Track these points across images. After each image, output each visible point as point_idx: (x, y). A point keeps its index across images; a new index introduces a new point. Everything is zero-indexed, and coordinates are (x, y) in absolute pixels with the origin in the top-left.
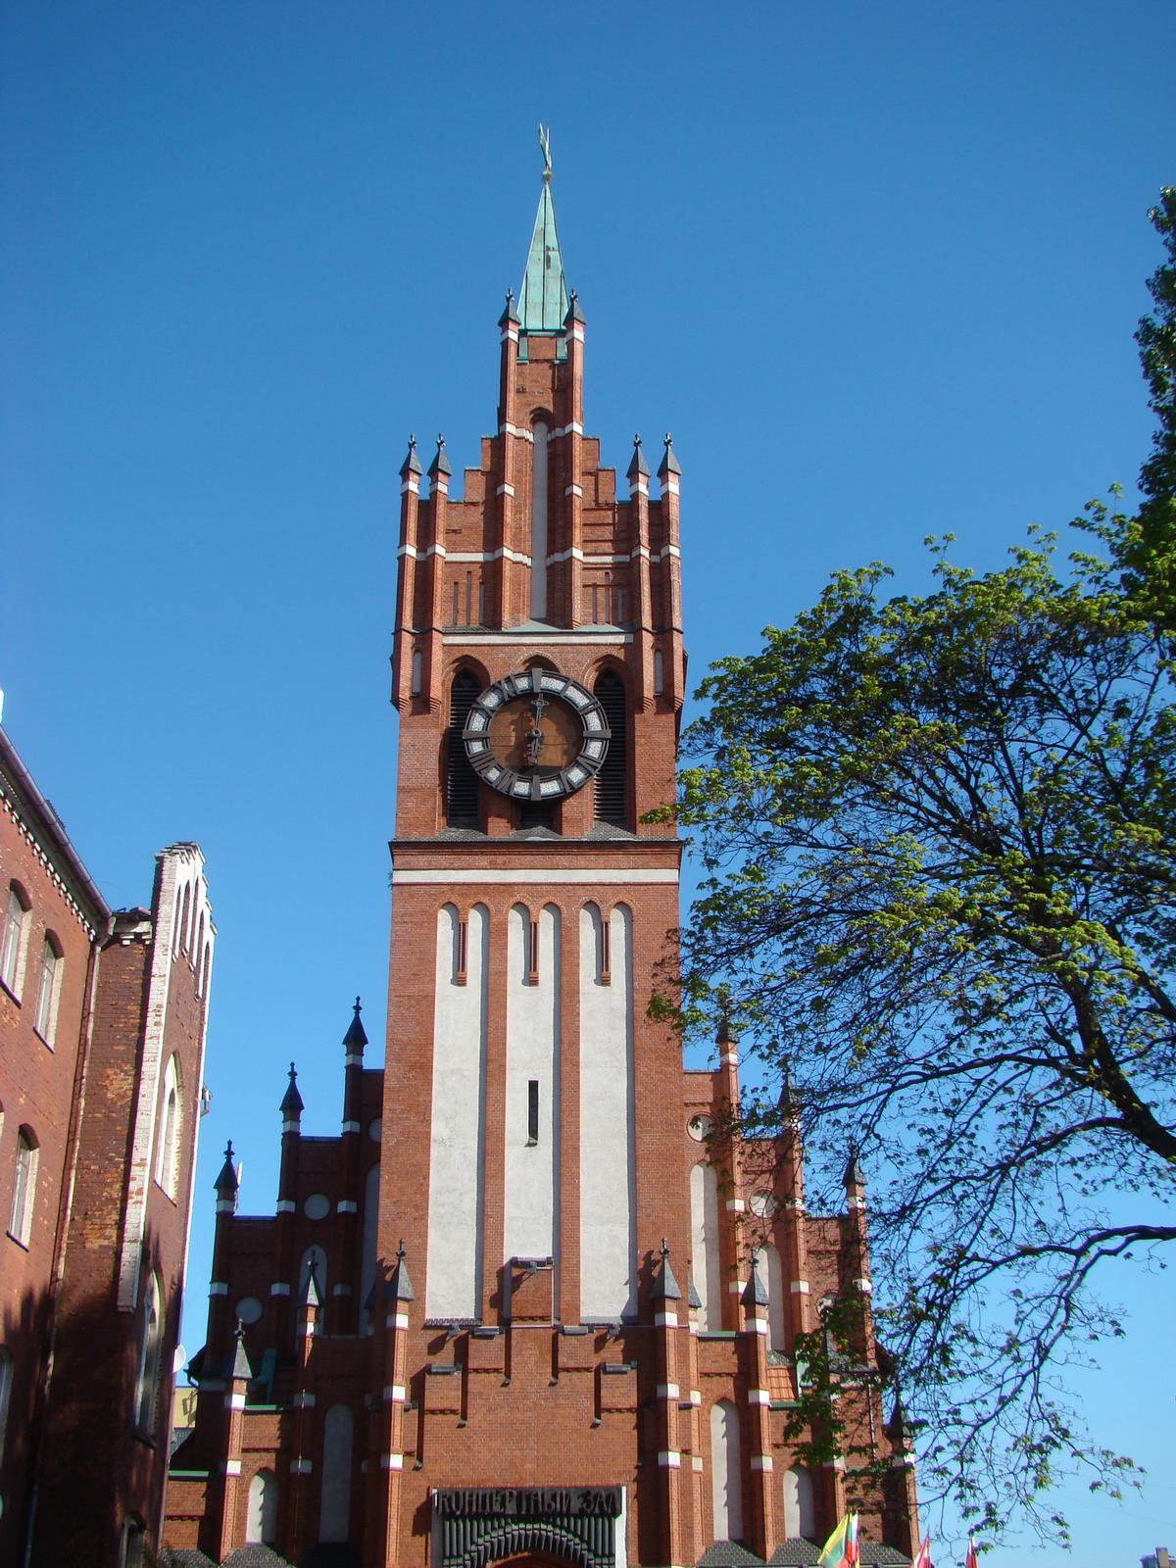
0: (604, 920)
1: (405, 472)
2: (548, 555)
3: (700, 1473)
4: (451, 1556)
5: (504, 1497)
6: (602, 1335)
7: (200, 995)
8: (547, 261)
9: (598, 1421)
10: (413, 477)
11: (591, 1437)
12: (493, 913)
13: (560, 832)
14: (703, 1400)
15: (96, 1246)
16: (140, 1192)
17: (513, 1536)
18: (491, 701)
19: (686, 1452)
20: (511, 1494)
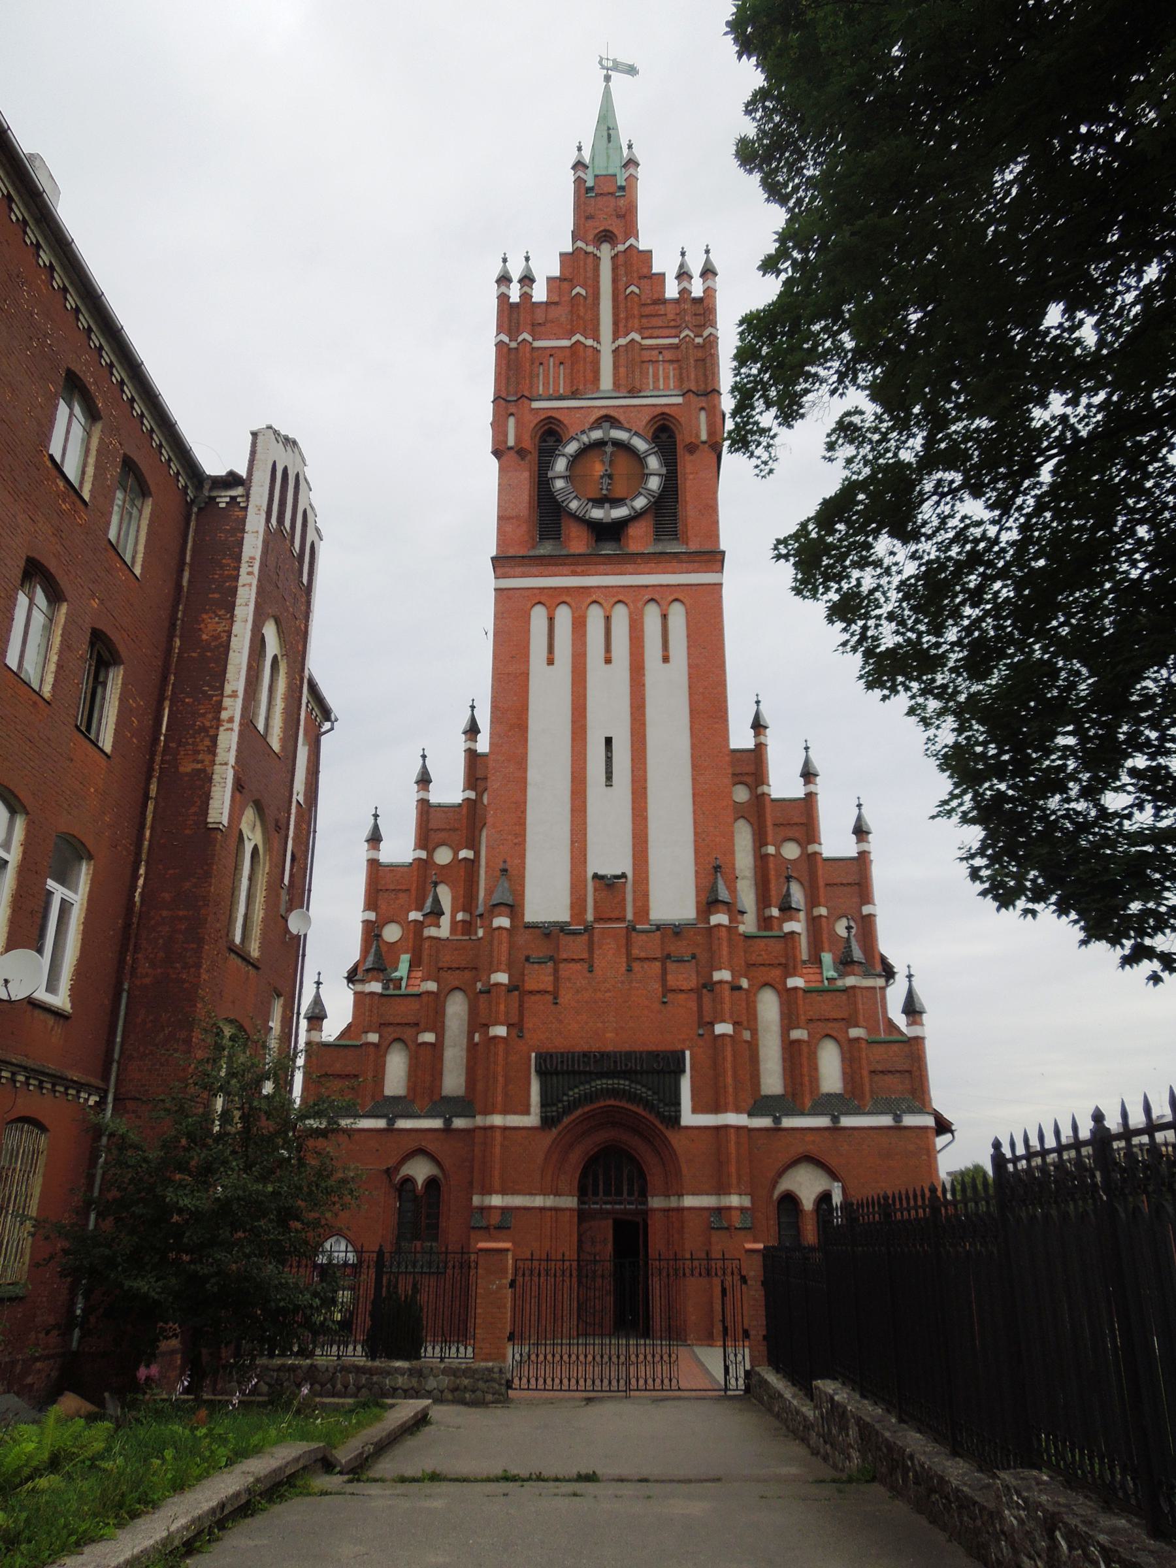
2: (613, 342)
14: (749, 985)
15: (189, 770)
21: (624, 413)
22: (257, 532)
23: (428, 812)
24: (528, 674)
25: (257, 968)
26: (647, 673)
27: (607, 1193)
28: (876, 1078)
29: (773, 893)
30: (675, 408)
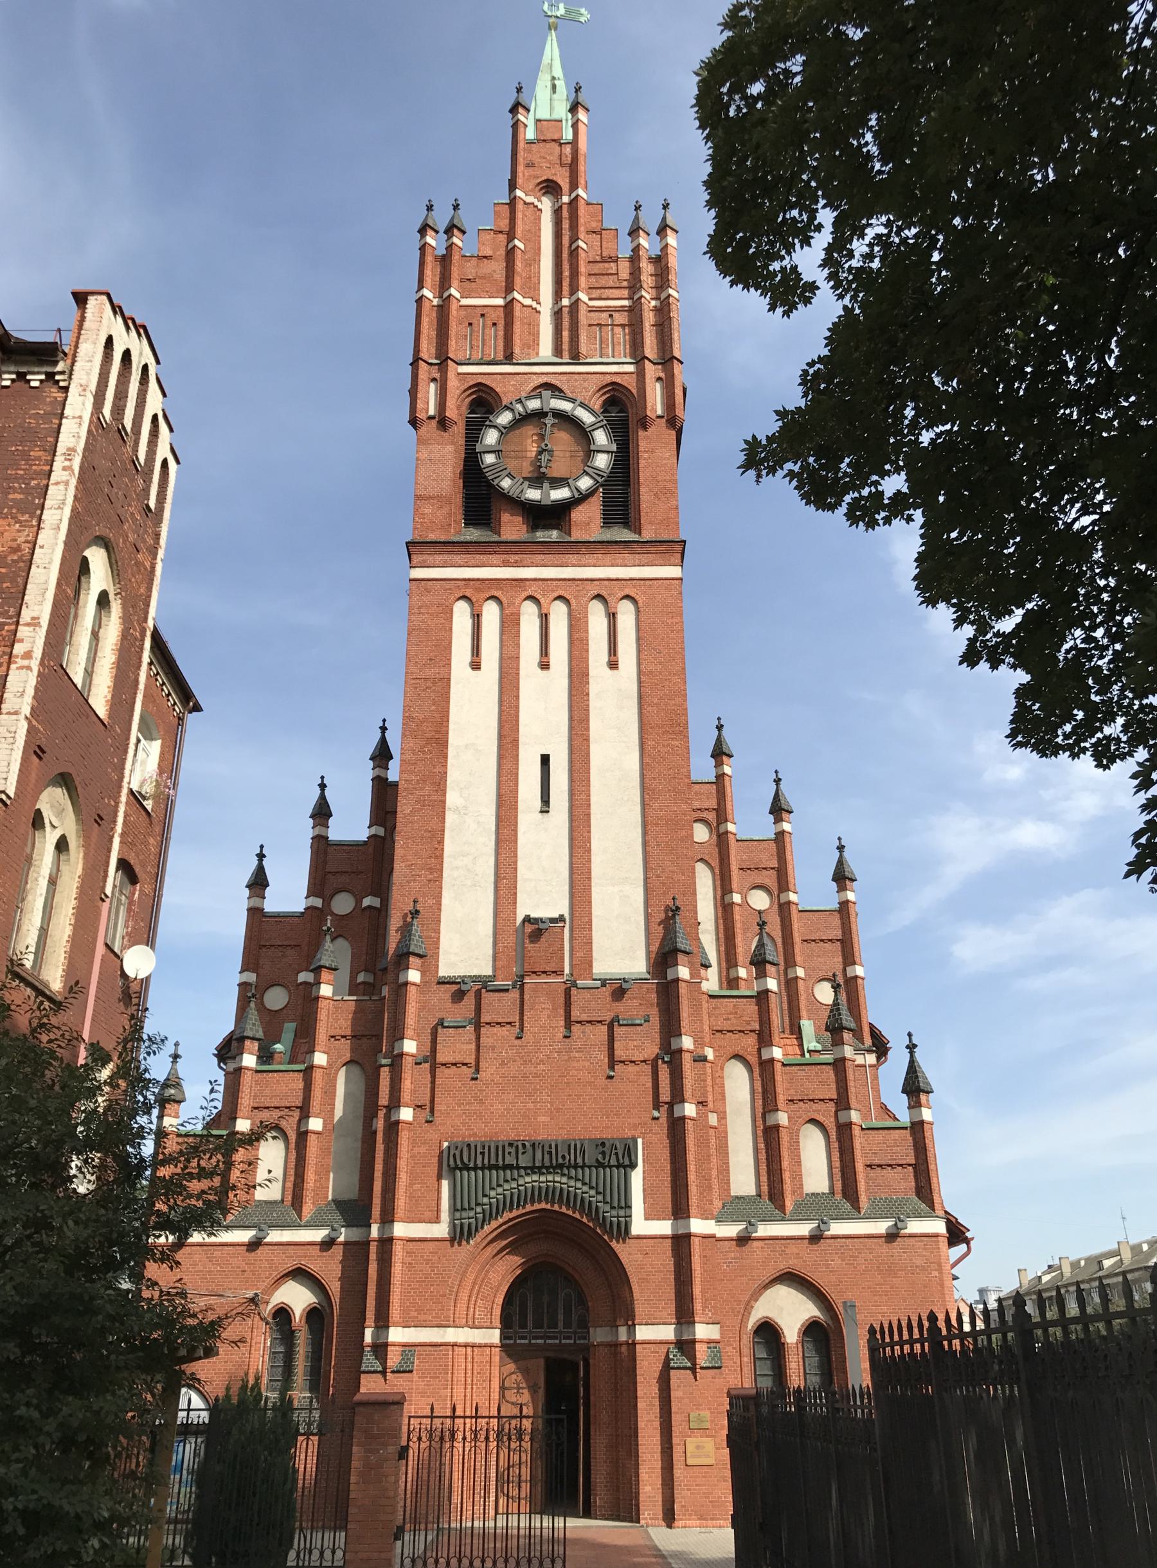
4: (463, 1209)
6: (619, 989)
7: (152, 504)
8: (554, 87)
10: (430, 232)
11: (605, 1089)
13: (570, 535)
16: (28, 655)
17: (526, 1188)
18: (505, 418)
19: (701, 1103)
21: (568, 381)
22: (80, 417)
23: (326, 852)
24: (449, 679)
26: (591, 681)
28: (872, 1173)
29: (740, 950)
30: (626, 377)
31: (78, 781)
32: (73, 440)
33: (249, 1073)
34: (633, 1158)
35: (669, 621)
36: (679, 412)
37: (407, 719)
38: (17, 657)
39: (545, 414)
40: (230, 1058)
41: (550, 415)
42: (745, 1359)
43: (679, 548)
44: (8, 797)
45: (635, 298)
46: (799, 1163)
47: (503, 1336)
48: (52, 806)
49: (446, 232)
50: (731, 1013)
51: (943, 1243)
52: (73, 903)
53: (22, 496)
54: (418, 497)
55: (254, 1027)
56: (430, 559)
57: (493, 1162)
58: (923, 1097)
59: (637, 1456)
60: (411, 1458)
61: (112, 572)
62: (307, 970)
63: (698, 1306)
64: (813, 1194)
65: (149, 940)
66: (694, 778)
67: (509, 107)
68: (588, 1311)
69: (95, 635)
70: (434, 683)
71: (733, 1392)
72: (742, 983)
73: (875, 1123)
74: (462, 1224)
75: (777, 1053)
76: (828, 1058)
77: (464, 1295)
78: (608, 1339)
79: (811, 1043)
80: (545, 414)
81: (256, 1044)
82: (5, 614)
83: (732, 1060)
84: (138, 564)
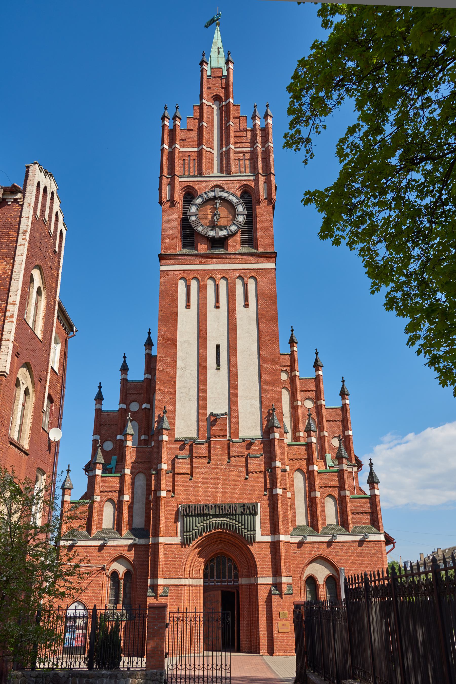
0: (246, 283)
1: (163, 118)
3: (290, 498)
4: (187, 532)
5: (209, 507)
6: (249, 443)
7: (57, 249)
8: (218, 52)
9: (247, 477)
10: (166, 119)
11: (245, 483)
12: (201, 281)
13: (227, 250)
16: (12, 316)
17: (213, 523)
18: (199, 201)
19: (284, 489)
20: (212, 506)
21: (226, 184)
22: (28, 217)
23: (127, 385)
24: (177, 313)
25: (27, 454)
27: (218, 577)
28: (354, 516)
29: (301, 425)
31: (32, 365)
32: (25, 227)
33: (99, 477)
34: (256, 510)
35: (270, 287)
36: (274, 197)
37: (160, 330)
38: (8, 317)
39: (216, 199)
40: (90, 470)
41: (219, 199)
42: (302, 591)
43: (274, 256)
44: (7, 374)
45: (255, 147)
46: (324, 512)
47: (204, 582)
48: (23, 376)
49: (173, 119)
50: (297, 452)
51: (383, 544)
52: (32, 414)
53: (6, 251)
54: (163, 235)
55: (100, 458)
56: (168, 262)
57: (199, 512)
58: (376, 485)
59: (259, 629)
60: (170, 628)
61: (42, 279)
62: (121, 434)
63: (283, 569)
64: (330, 525)
65: (59, 426)
66: (281, 353)
67: (199, 62)
68: (238, 571)
69: (36, 305)
70: (171, 315)
71: (296, 603)
72: (302, 439)
73: (356, 496)
74: (187, 538)
75: (316, 468)
76: (336, 469)
77: (188, 566)
78: (247, 582)
79: (330, 463)
80: (216, 199)
81: (101, 465)
82: (1, 299)
83: (297, 472)
84: (52, 275)
